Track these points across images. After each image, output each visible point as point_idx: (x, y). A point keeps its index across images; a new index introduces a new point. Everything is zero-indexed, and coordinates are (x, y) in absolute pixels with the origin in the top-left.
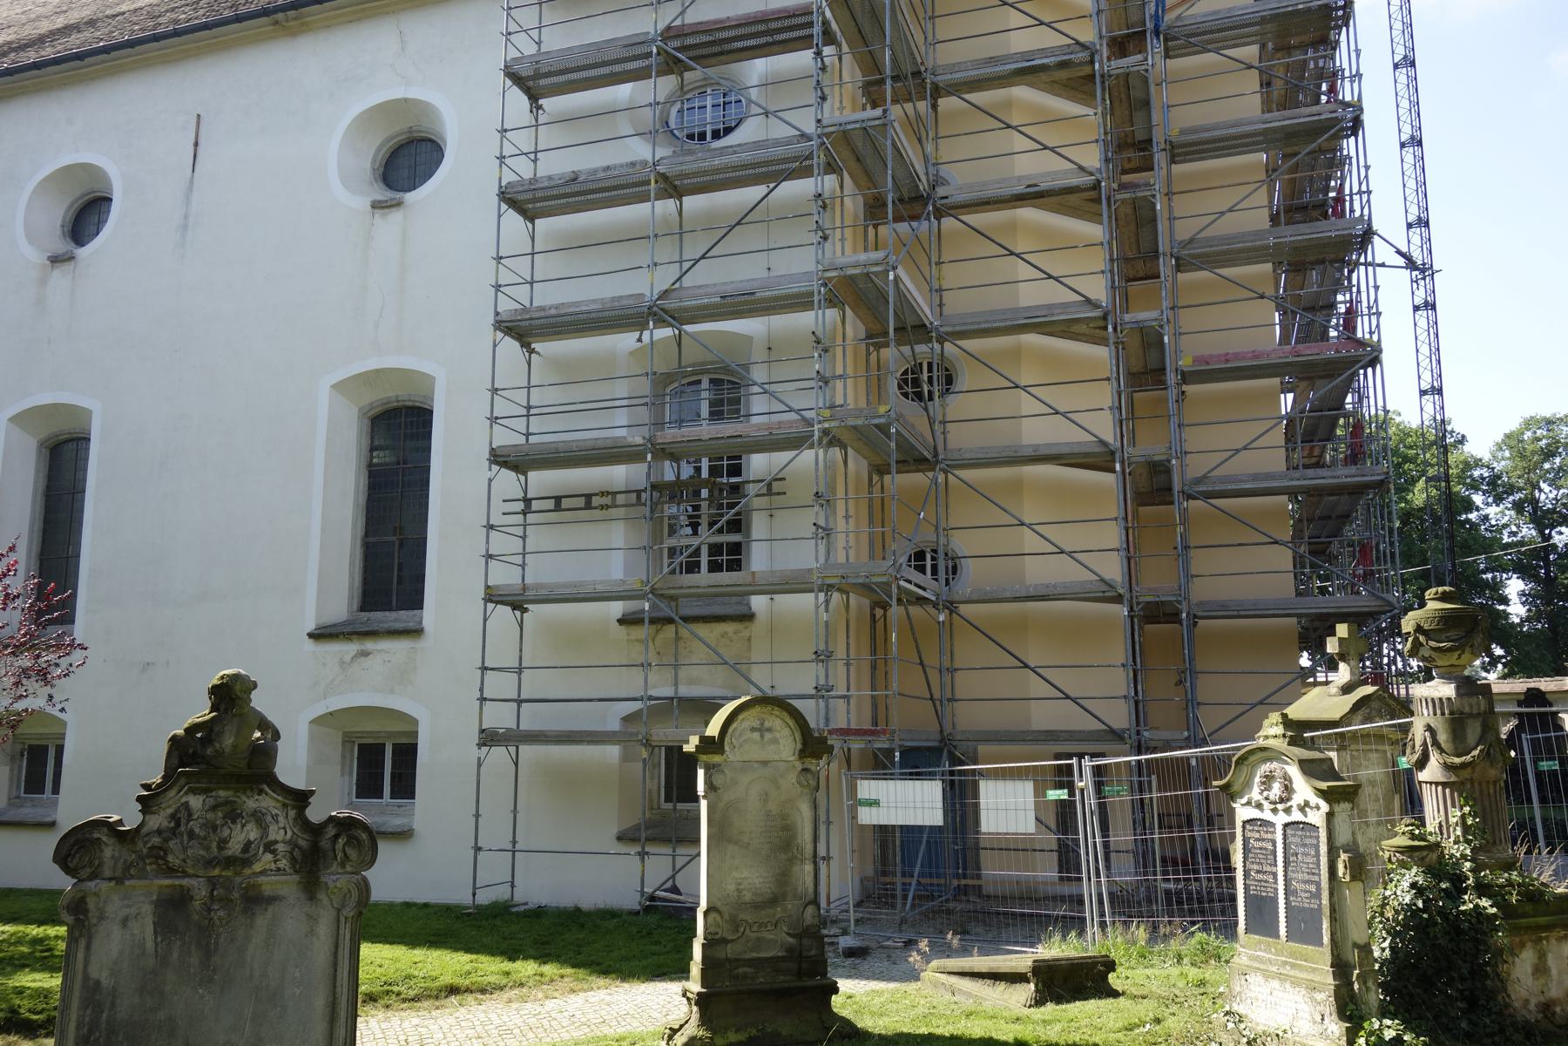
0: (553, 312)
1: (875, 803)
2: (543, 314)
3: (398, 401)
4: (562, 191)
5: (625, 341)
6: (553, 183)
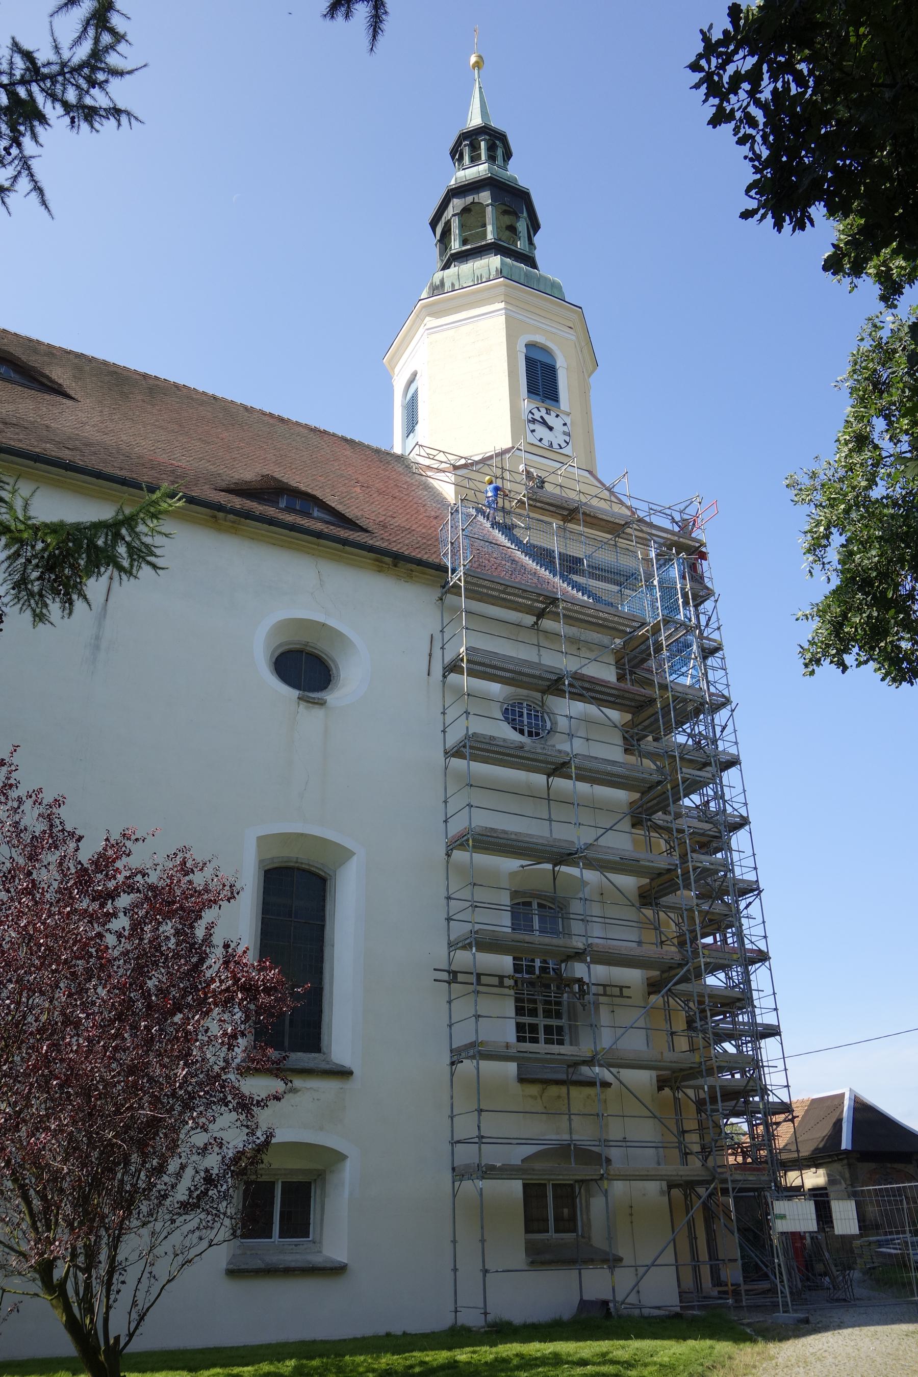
0: (513, 837)
1: (783, 1217)
2: (506, 836)
3: (297, 862)
4: (512, 752)
5: (512, 864)
6: (506, 745)
